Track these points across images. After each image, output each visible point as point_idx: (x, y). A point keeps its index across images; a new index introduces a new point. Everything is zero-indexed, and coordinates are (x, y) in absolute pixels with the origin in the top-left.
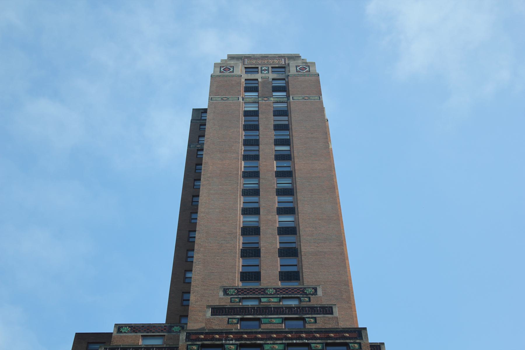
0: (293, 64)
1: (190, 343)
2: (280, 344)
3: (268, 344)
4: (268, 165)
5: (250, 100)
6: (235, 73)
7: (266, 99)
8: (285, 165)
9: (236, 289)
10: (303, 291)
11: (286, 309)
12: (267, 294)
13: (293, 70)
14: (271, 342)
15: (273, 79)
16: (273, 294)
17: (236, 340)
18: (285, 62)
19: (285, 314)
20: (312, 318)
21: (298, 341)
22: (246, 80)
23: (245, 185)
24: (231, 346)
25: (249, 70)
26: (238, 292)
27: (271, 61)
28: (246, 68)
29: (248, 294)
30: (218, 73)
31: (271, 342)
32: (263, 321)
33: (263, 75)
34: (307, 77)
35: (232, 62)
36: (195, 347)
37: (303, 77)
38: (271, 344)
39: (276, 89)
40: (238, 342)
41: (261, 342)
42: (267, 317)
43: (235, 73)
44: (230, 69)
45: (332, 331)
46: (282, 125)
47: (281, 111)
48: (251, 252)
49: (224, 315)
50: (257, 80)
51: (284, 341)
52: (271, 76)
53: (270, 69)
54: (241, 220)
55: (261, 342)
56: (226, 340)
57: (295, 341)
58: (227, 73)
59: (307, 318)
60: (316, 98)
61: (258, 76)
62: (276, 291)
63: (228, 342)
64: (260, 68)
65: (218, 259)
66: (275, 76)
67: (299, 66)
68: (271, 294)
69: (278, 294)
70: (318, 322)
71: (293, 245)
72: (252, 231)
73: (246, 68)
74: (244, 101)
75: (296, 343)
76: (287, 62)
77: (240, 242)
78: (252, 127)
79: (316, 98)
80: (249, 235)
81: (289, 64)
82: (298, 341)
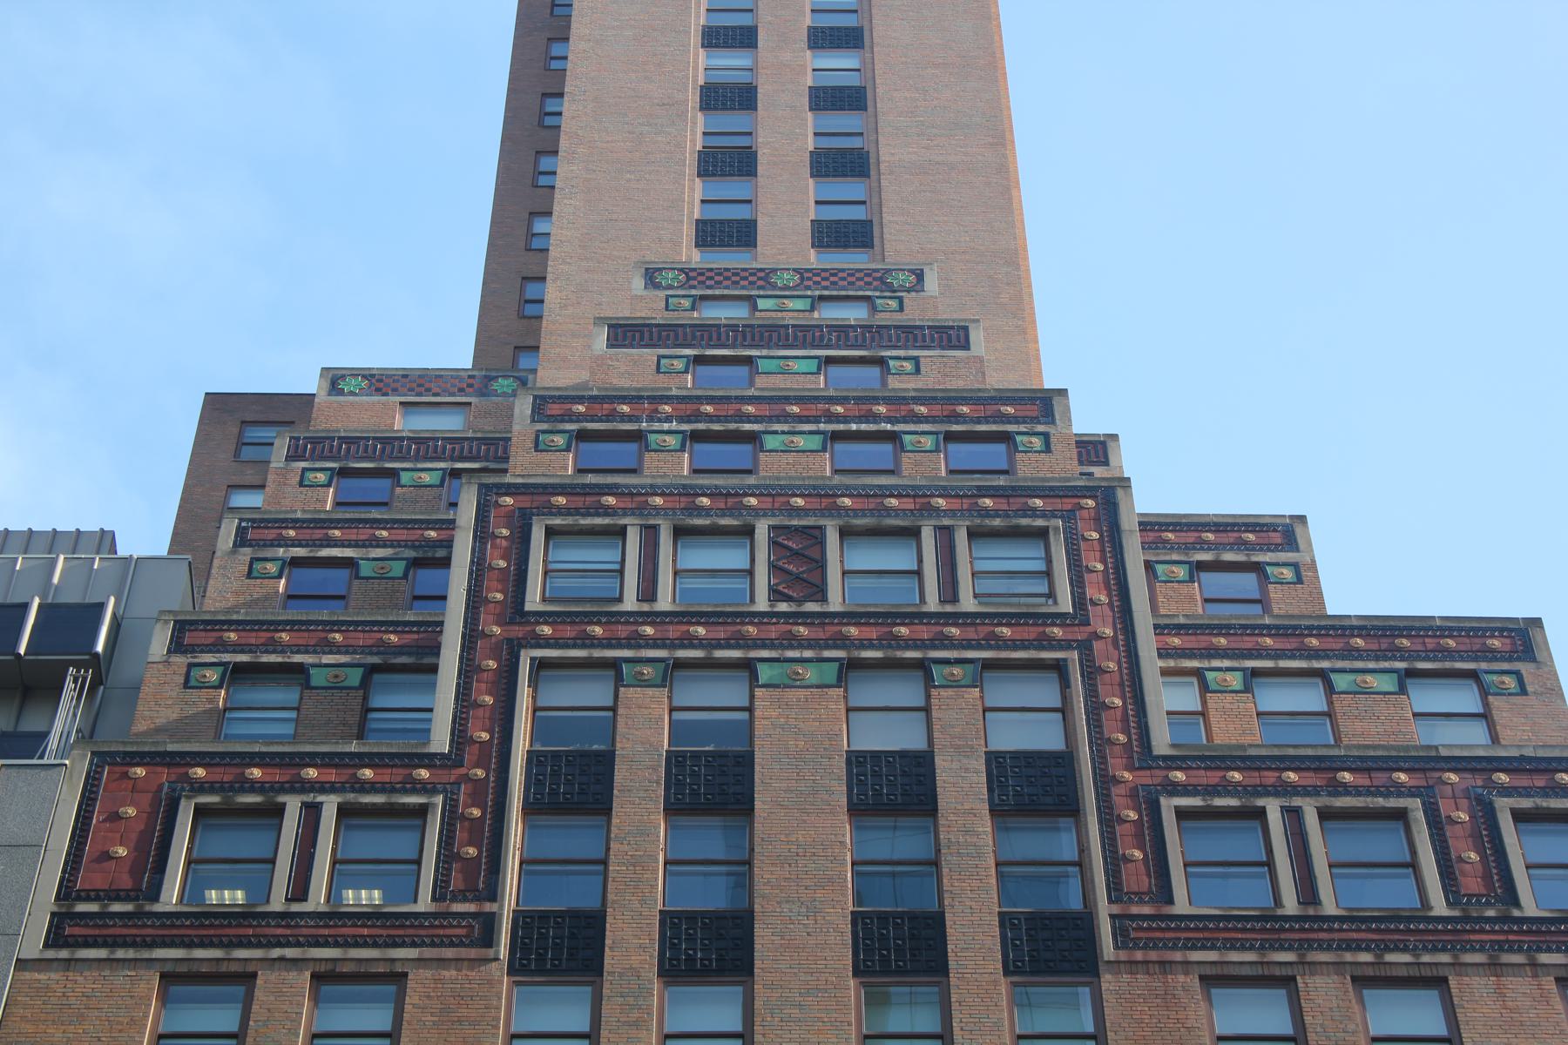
2: (811, 433)
3: (775, 432)
9: (681, 270)
10: (881, 279)
12: (774, 286)
14: (786, 427)
17: (681, 420)
19: (828, 347)
24: (667, 438)
38: (783, 433)
40: (686, 427)
48: (728, 161)
54: (701, 64)
57: (854, 427)
62: (802, 279)
65: (629, 181)
68: (786, 288)
71: (856, 143)
77: (694, 130)
80: (724, 108)
82: (864, 427)
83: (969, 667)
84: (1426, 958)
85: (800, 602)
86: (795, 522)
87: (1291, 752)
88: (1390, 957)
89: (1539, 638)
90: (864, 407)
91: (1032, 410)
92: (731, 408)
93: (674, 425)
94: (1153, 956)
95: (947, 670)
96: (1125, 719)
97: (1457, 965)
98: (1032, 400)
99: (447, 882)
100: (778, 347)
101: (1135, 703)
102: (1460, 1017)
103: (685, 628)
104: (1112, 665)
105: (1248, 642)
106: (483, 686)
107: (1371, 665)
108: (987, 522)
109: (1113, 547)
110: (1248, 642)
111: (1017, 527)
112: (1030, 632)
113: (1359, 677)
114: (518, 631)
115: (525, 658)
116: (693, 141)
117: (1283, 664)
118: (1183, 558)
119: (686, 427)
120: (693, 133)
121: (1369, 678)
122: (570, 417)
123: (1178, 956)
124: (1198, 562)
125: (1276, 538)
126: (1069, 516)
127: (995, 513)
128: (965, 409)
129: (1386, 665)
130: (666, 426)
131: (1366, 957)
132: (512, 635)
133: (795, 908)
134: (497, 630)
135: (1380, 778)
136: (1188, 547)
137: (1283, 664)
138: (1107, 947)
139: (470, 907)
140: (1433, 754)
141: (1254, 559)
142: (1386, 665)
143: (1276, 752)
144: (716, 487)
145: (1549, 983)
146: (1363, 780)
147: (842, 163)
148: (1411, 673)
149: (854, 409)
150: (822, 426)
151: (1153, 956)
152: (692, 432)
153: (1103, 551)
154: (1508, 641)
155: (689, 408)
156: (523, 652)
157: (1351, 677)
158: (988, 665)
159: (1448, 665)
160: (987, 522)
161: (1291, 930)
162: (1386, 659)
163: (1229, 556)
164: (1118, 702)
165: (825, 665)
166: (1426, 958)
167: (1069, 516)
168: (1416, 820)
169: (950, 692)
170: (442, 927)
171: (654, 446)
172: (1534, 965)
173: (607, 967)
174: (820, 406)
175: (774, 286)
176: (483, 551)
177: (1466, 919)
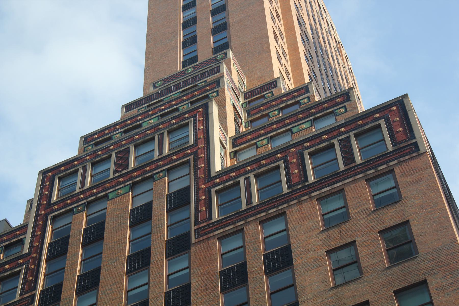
2: (155, 117)
9: (163, 80)
10: (215, 60)
12: (187, 74)
14: (148, 119)
16: (192, 72)
17: (121, 128)
19: (183, 87)
20: (270, 93)
24: (117, 135)
26: (164, 81)
32: (294, 130)
38: (148, 120)
40: (122, 130)
45: (311, 107)
48: (190, 41)
54: (181, 17)
56: (114, 132)
57: (166, 111)
59: (336, 110)
63: (115, 133)
68: (190, 73)
69: (196, 70)
70: (348, 110)
72: (190, 23)
75: (168, 112)
77: (181, 36)
82: (169, 110)
83: (164, 172)
84: (280, 208)
85: (121, 171)
86: (122, 149)
87: (249, 161)
88: (270, 211)
90: (169, 104)
91: (215, 85)
92: (134, 120)
93: (120, 131)
94: (205, 237)
95: (158, 175)
96: (204, 170)
97: (289, 206)
99: (24, 290)
100: (169, 93)
101: (207, 164)
102: (288, 222)
103: (91, 192)
104: (202, 155)
105: (269, 129)
106: (39, 230)
107: (303, 121)
108: (173, 127)
109: (206, 120)
110: (269, 129)
111: (181, 125)
112: (181, 155)
113: (299, 127)
114: (209, 185)
115: (213, 191)
116: (180, 40)
117: (279, 131)
118: (277, 108)
120: (180, 37)
121: (302, 126)
122: (93, 140)
123: (212, 235)
126: (194, 116)
127: (176, 123)
128: (196, 93)
130: (117, 132)
131: (264, 214)
132: (208, 186)
133: (112, 261)
134: (203, 186)
135: (273, 158)
136: (277, 105)
137: (279, 131)
138: (193, 239)
139: (29, 294)
140: (288, 145)
141: (297, 100)
143: (245, 162)
144: (103, 147)
145: (315, 201)
146: (268, 161)
147: (220, 28)
148: (315, 119)
149: (167, 105)
150: (158, 114)
151: (205, 237)
153: (203, 122)
154: (343, 98)
156: (212, 190)
158: (169, 169)
159: (325, 112)
160: (173, 127)
161: (244, 214)
162: (307, 118)
164: (203, 165)
165: (126, 187)
166: (280, 208)
167: (194, 116)
168: (282, 167)
169: (159, 181)
170: (22, 303)
172: (310, 197)
173: (62, 298)
174: (158, 109)
175: (187, 74)
176: (42, 191)
177: (293, 191)
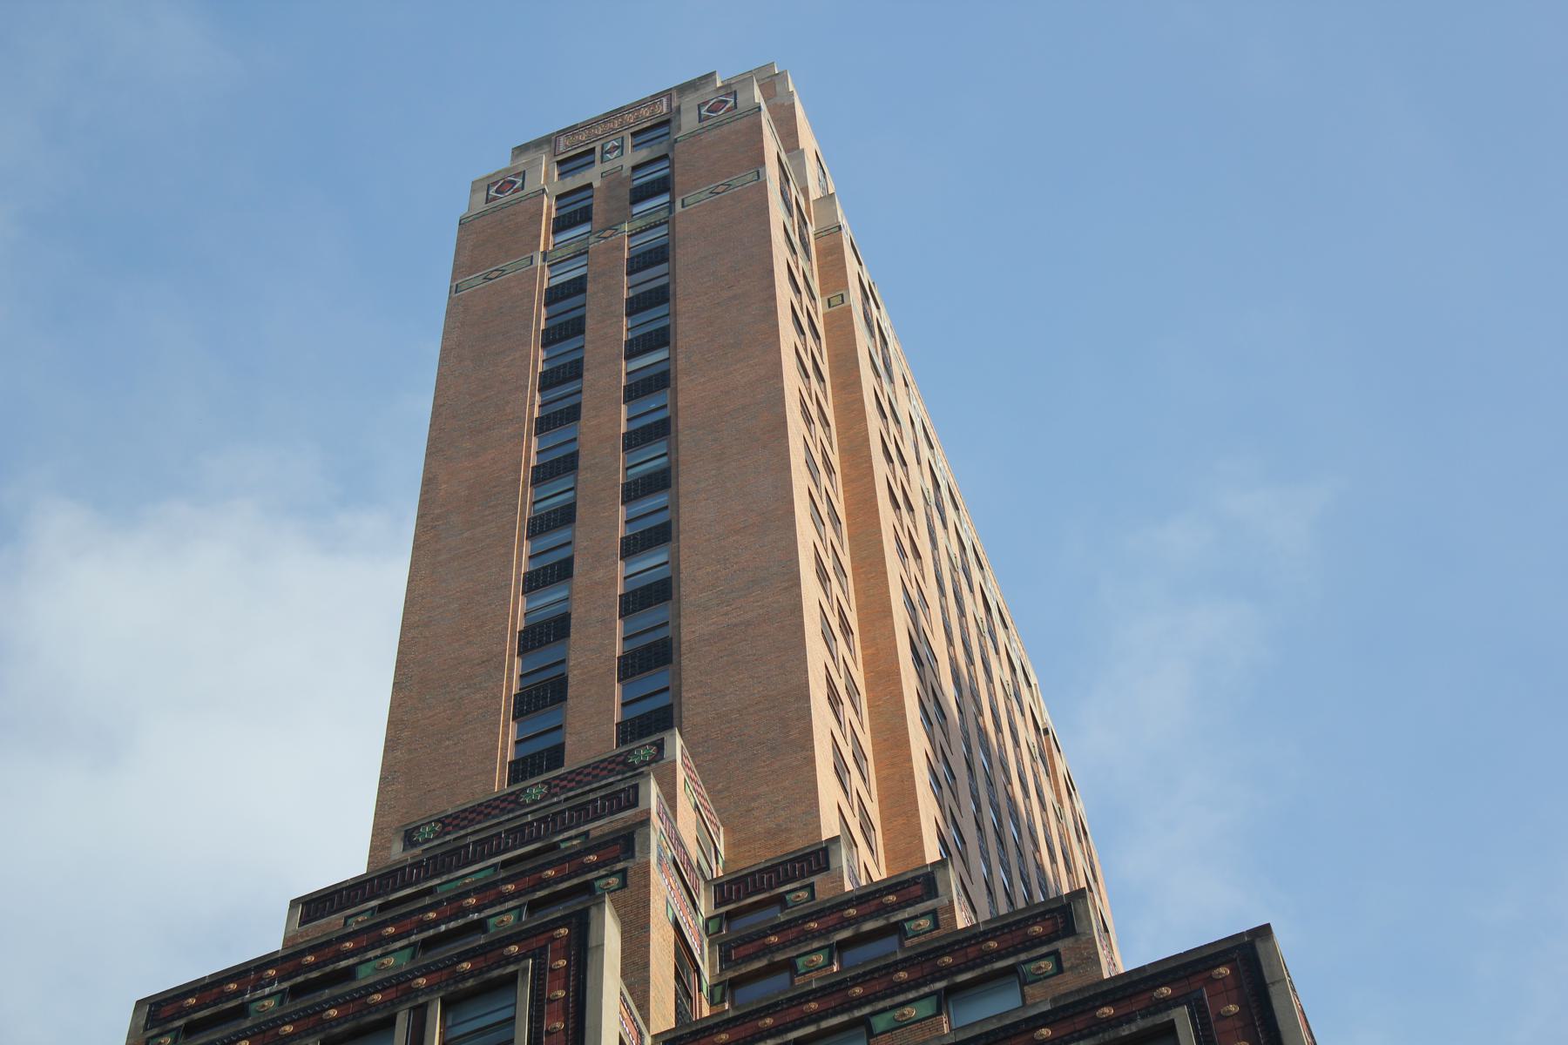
0: (689, 103)
1: (155, 1031)
2: (402, 948)
3: (369, 960)
4: (608, 417)
5: (565, 251)
6: (528, 189)
7: (609, 232)
8: (653, 406)
9: (438, 821)
10: (624, 763)
11: (507, 837)
12: (524, 805)
13: (689, 121)
14: (378, 952)
15: (635, 168)
17: (282, 980)
18: (669, 105)
21: (452, 925)
22: (558, 198)
23: (538, 506)
25: (567, 165)
27: (630, 118)
28: (560, 163)
29: (472, 822)
30: (481, 206)
31: (378, 952)
33: (607, 166)
34: (725, 129)
35: (523, 160)
36: (167, 1040)
37: (717, 131)
39: (639, 195)
40: (285, 985)
41: (1010, 961)
42: (452, 876)
43: (528, 189)
44: (514, 183)
46: (650, 291)
47: (650, 251)
48: (543, 695)
49: (335, 912)
50: (590, 186)
51: (413, 938)
52: (631, 157)
53: (629, 142)
54: (519, 610)
55: (1010, 961)
57: (443, 928)
58: (507, 197)
60: (749, 177)
61: (593, 176)
62: (549, 789)
63: (259, 993)
64: (598, 150)
65: (447, 747)
66: (643, 155)
67: (705, 103)
68: (535, 802)
69: (555, 795)
71: (660, 635)
72: (546, 634)
73: (560, 163)
74: (543, 262)
76: (674, 105)
78: (565, 332)
79: (749, 177)
80: (541, 645)
81: (679, 108)
82: (452, 925)
89: (1081, 909)
98: (615, 841)
107: (911, 996)
111: (490, 980)
113: (897, 1013)
119: (285, 985)
124: (838, 942)
125: (917, 890)
126: (539, 955)
129: (926, 990)
141: (893, 920)
142: (926, 990)
152: (291, 987)
153: (567, 977)
154: (1049, 923)
155: (289, 965)
157: (889, 1015)
162: (925, 984)
163: (869, 926)
167: (539, 955)
171: (1030, 978)
175: (524, 805)
